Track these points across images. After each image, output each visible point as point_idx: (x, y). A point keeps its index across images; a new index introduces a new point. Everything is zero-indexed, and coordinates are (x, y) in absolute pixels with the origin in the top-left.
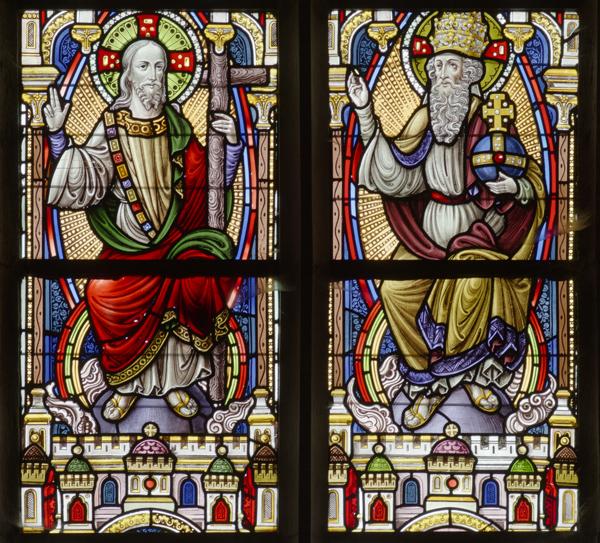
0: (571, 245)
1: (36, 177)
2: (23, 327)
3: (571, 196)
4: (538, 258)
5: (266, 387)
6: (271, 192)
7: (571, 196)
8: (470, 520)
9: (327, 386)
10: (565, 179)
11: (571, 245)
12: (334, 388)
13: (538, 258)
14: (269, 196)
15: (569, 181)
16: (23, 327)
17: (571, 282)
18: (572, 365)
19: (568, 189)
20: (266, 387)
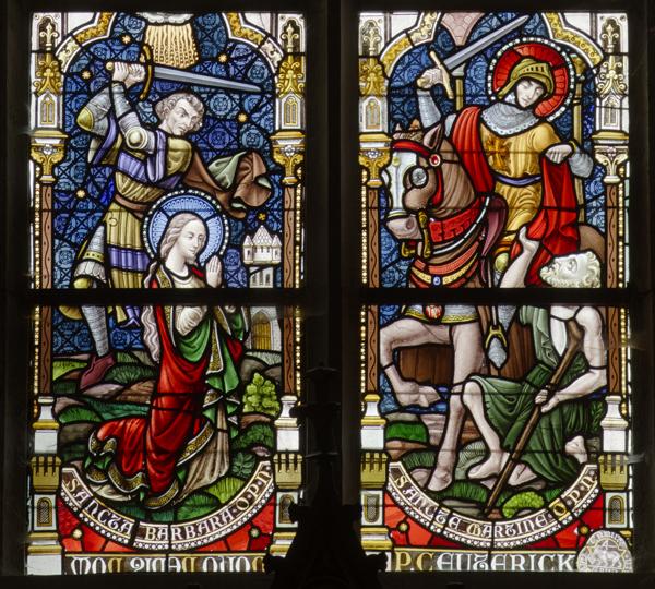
0: (364, 267)
1: (45, 207)
2: (631, 494)
3: (364, 213)
4: (119, 570)
5: (42, 184)
6: (37, 206)
7: (364, 213)
8: (593, 54)
9: (360, 388)
10: (45, 214)
11: (364, 267)
12: (367, 392)
13: (119, 570)
14: (41, 201)
15: (41, 211)
16: (631, 494)
17: (623, 311)
18: (623, 317)
19: (366, 386)
20: (42, 184)
